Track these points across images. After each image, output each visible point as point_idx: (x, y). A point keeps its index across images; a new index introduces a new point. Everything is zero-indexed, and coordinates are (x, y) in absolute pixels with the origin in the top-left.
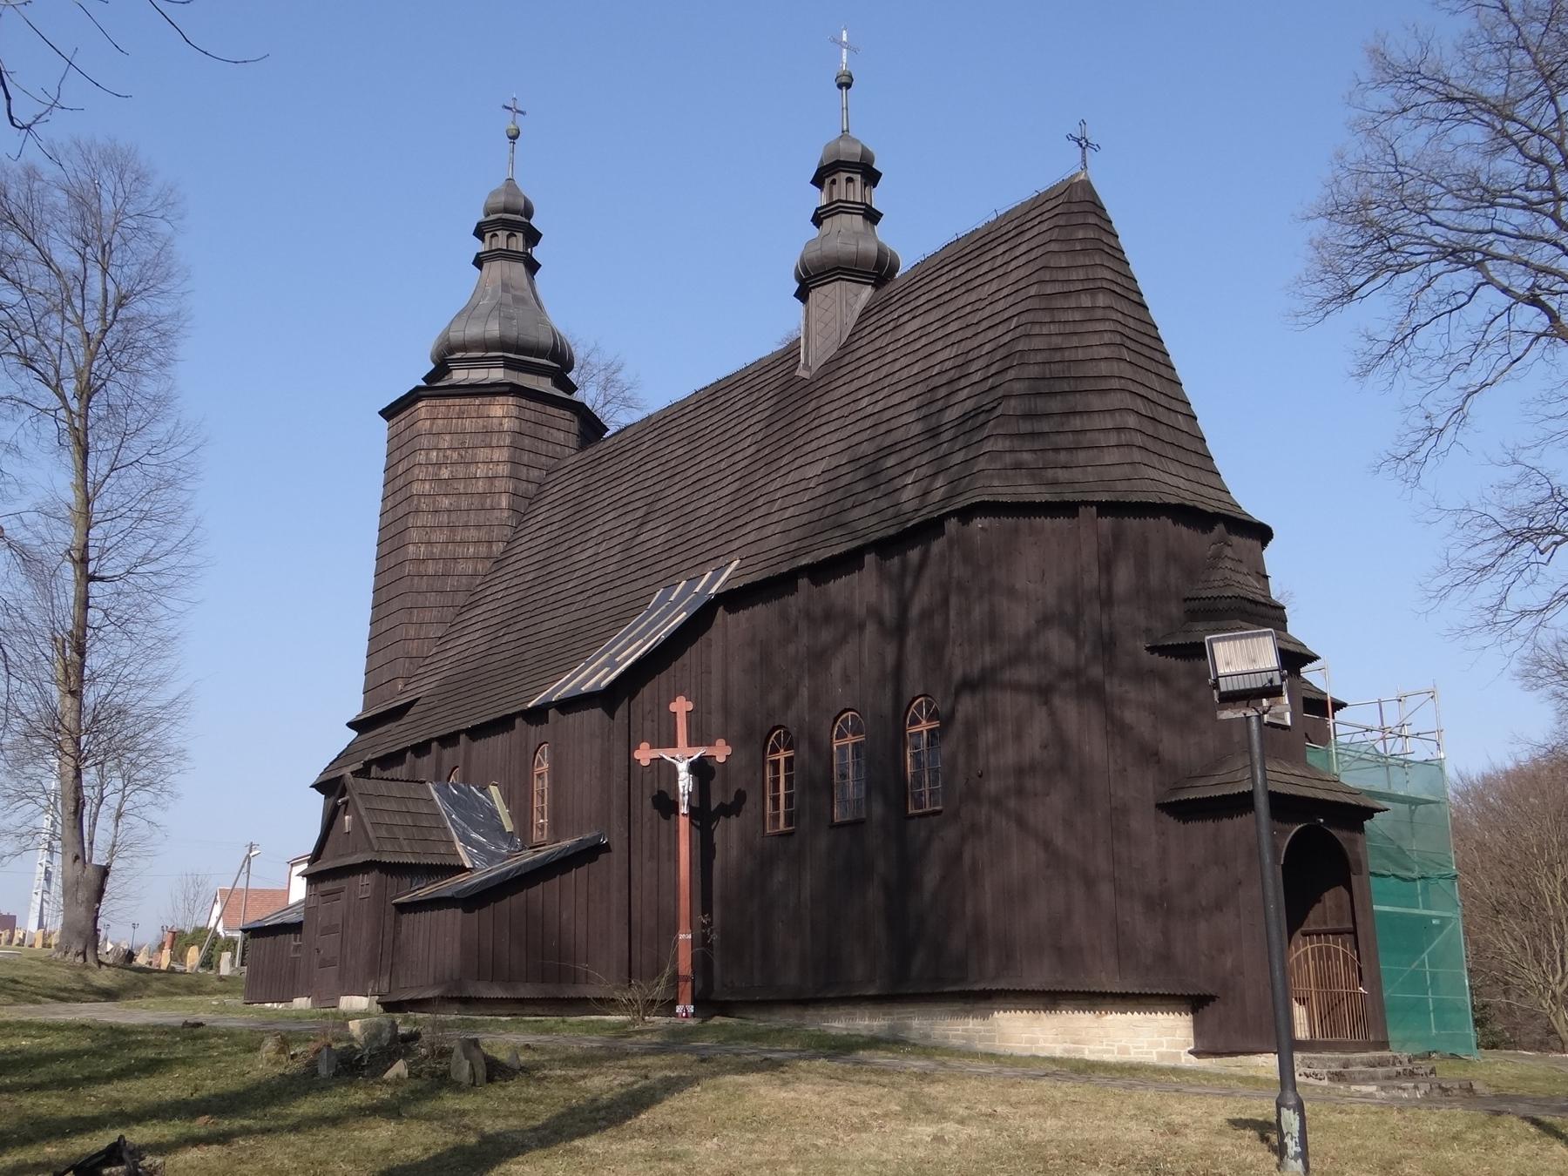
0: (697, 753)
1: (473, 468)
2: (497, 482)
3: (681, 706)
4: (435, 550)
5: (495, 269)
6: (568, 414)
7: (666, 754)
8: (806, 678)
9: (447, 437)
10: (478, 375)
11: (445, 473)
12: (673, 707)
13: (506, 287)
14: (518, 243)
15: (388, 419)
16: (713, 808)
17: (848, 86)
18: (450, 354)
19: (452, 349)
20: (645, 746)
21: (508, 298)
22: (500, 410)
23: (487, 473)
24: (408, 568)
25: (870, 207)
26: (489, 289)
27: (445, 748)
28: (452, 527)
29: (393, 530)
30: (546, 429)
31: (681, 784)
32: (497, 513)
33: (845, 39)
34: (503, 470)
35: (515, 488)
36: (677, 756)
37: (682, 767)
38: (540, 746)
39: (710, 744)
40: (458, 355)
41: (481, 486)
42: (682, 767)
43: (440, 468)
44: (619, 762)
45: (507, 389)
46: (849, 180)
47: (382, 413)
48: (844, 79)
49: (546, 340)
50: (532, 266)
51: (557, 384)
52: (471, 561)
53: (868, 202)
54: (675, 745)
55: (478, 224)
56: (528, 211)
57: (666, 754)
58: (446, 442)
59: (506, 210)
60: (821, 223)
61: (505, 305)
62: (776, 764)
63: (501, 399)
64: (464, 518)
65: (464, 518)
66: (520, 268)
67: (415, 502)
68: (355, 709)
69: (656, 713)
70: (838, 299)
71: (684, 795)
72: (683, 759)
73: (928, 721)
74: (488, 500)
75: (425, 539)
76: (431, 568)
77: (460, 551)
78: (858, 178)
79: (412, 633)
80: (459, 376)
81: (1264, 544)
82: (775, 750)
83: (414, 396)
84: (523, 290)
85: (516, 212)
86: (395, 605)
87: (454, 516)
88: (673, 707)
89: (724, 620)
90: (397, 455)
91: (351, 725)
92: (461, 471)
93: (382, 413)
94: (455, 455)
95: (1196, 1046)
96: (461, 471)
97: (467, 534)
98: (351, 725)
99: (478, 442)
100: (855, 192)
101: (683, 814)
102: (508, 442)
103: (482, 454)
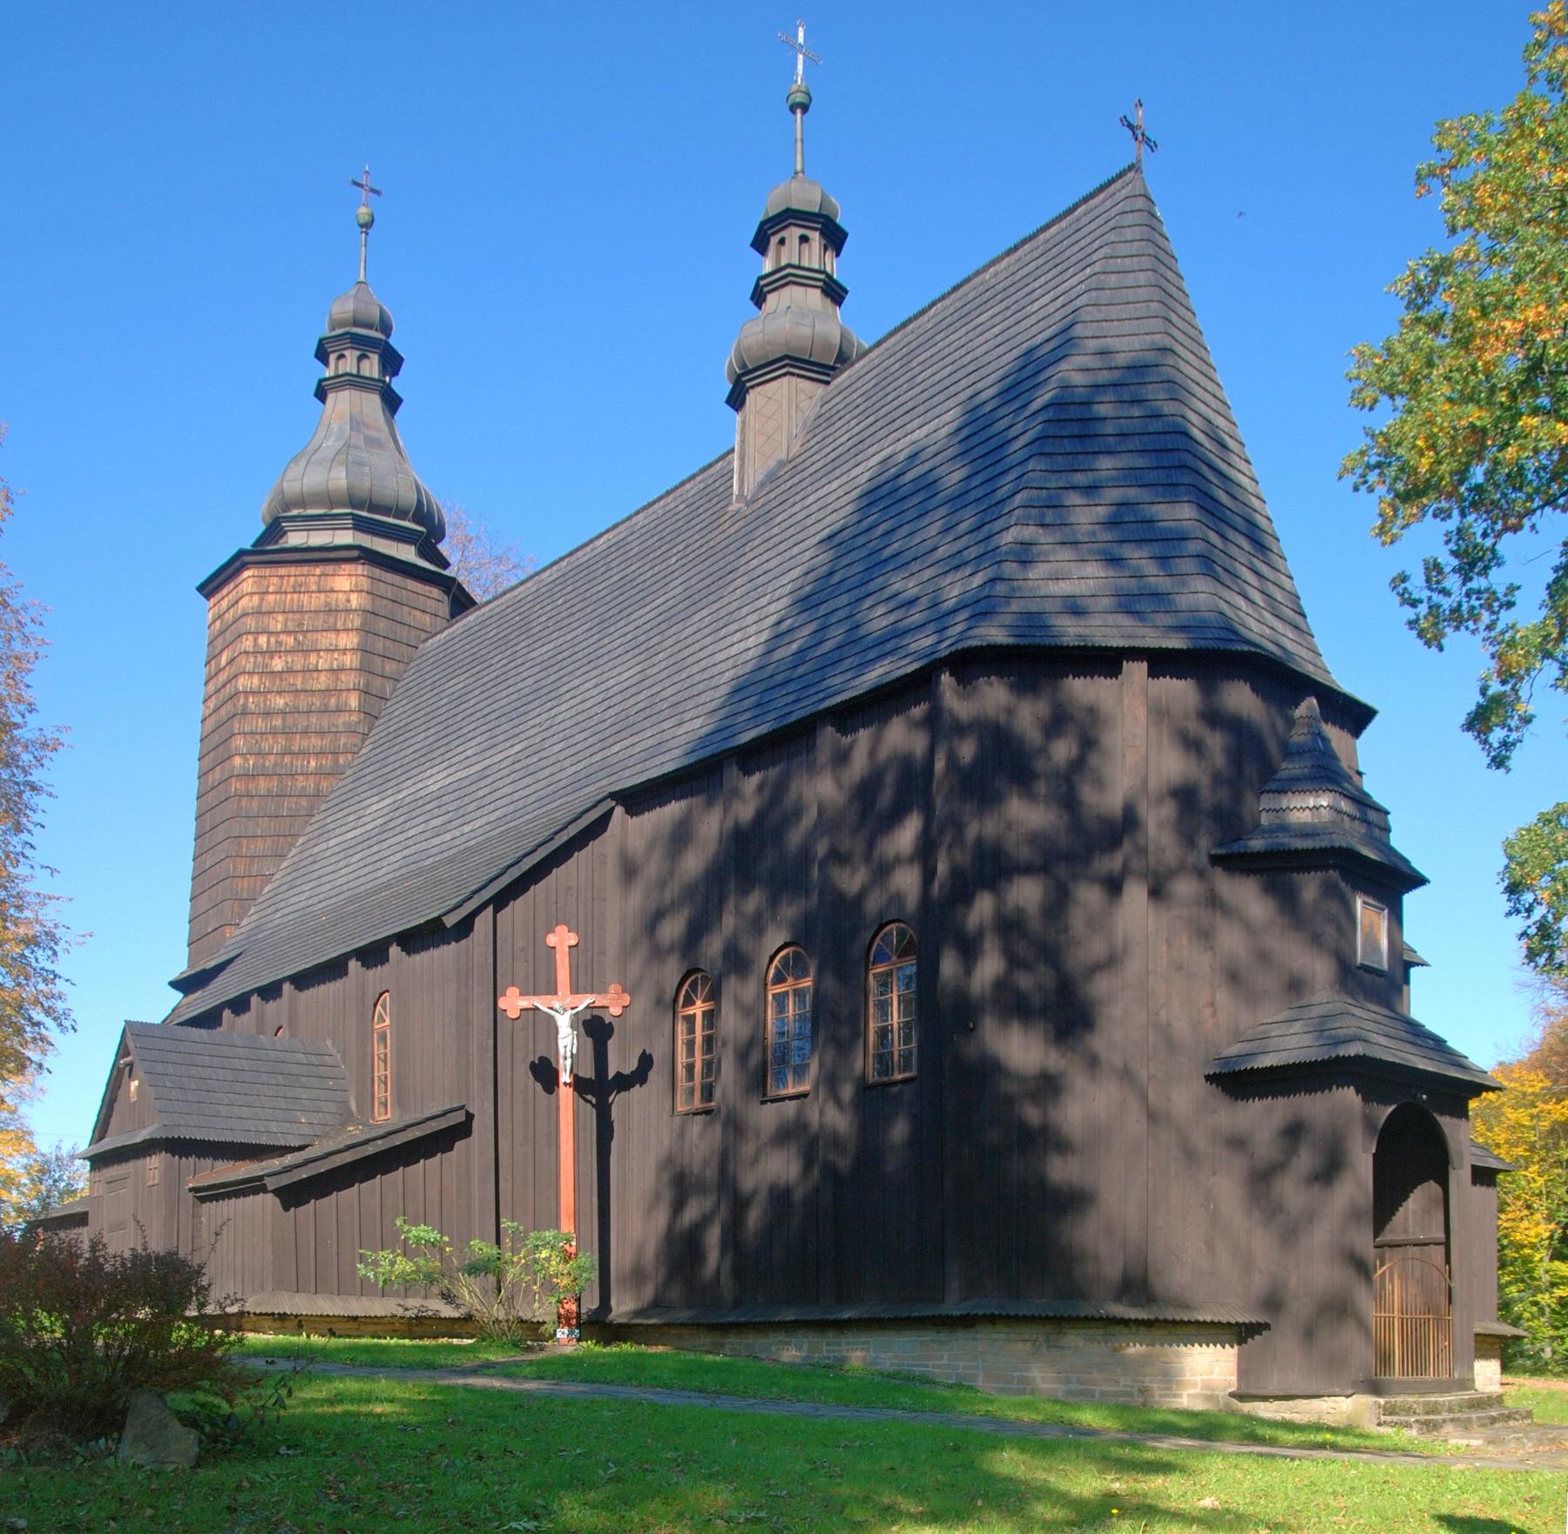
0: (585, 1001)
1: (313, 658)
2: (343, 677)
3: (562, 939)
4: (267, 764)
5: (341, 401)
6: (435, 592)
7: (540, 1002)
8: (733, 882)
9: (280, 618)
10: (319, 539)
11: (278, 664)
12: (552, 940)
13: (356, 424)
14: (372, 367)
15: (208, 597)
16: (610, 1077)
17: (805, 108)
18: (284, 511)
19: (287, 506)
20: (513, 992)
21: (358, 440)
22: (348, 583)
23: (332, 664)
24: (235, 786)
25: (830, 277)
26: (335, 427)
27: (267, 1001)
28: (288, 733)
29: (216, 739)
30: (406, 609)
31: (561, 1043)
32: (343, 718)
33: (801, 40)
34: (349, 660)
35: (367, 684)
36: (557, 1006)
37: (563, 1022)
38: (381, 995)
39: (603, 990)
40: (295, 512)
41: (323, 681)
42: (563, 1022)
43: (272, 658)
44: (482, 1019)
45: (355, 553)
46: (804, 239)
47: (201, 589)
48: (799, 98)
49: (410, 499)
50: (392, 402)
51: (422, 553)
52: (312, 778)
53: (828, 270)
54: (552, 990)
55: (321, 341)
56: (386, 327)
57: (540, 1002)
58: (277, 623)
59: (356, 323)
60: (764, 300)
61: (356, 447)
62: (690, 1020)
63: (347, 568)
64: (302, 722)
65: (302, 722)
66: (373, 401)
67: (242, 701)
68: (179, 965)
69: (531, 951)
70: (785, 402)
71: (565, 1058)
72: (565, 1010)
73: (899, 957)
74: (333, 701)
75: (256, 749)
76: (262, 785)
77: (299, 764)
78: (815, 236)
79: (241, 869)
80: (295, 539)
81: (1356, 731)
82: (689, 1002)
83: (237, 564)
84: (380, 430)
85: (369, 326)
86: (220, 833)
87: (290, 719)
88: (552, 940)
89: (624, 827)
90: (219, 643)
91: (175, 985)
92: (298, 662)
93: (201, 589)
94: (290, 641)
95: (1239, 1388)
96: (298, 662)
97: (305, 743)
98: (175, 985)
99: (319, 624)
100: (814, 255)
101: (565, 1084)
102: (357, 623)
103: (327, 640)
